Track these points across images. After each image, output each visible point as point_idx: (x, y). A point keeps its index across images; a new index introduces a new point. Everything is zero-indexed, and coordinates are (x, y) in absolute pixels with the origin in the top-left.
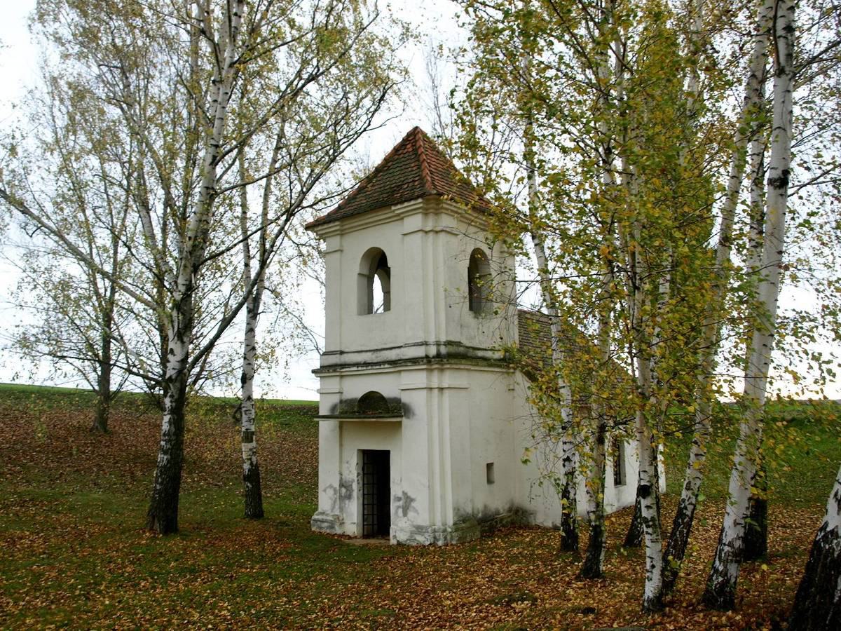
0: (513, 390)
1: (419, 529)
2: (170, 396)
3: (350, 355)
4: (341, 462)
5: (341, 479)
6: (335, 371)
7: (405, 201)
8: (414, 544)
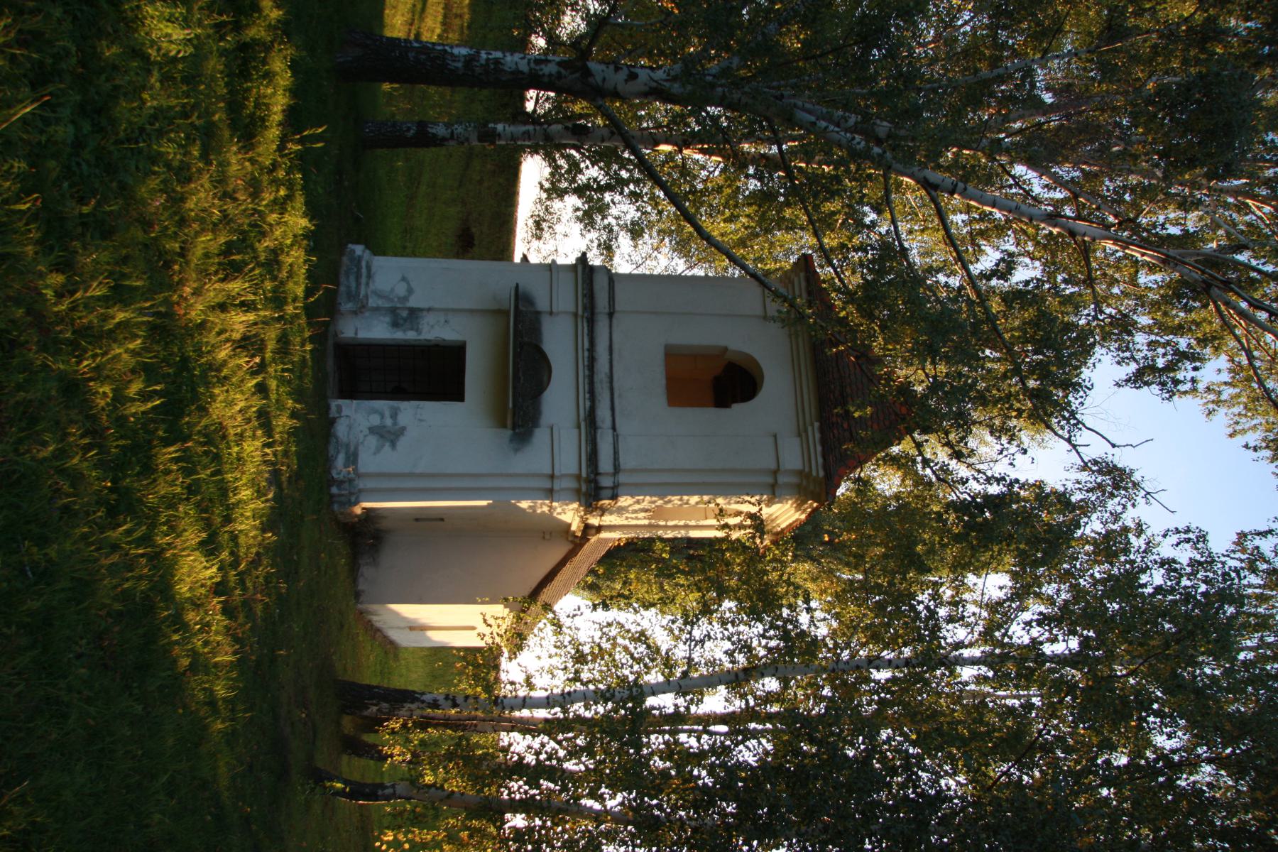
0: (544, 538)
1: (352, 458)
2: (559, 73)
3: (607, 330)
4: (446, 311)
5: (421, 310)
6: (585, 308)
7: (823, 449)
8: (332, 451)
